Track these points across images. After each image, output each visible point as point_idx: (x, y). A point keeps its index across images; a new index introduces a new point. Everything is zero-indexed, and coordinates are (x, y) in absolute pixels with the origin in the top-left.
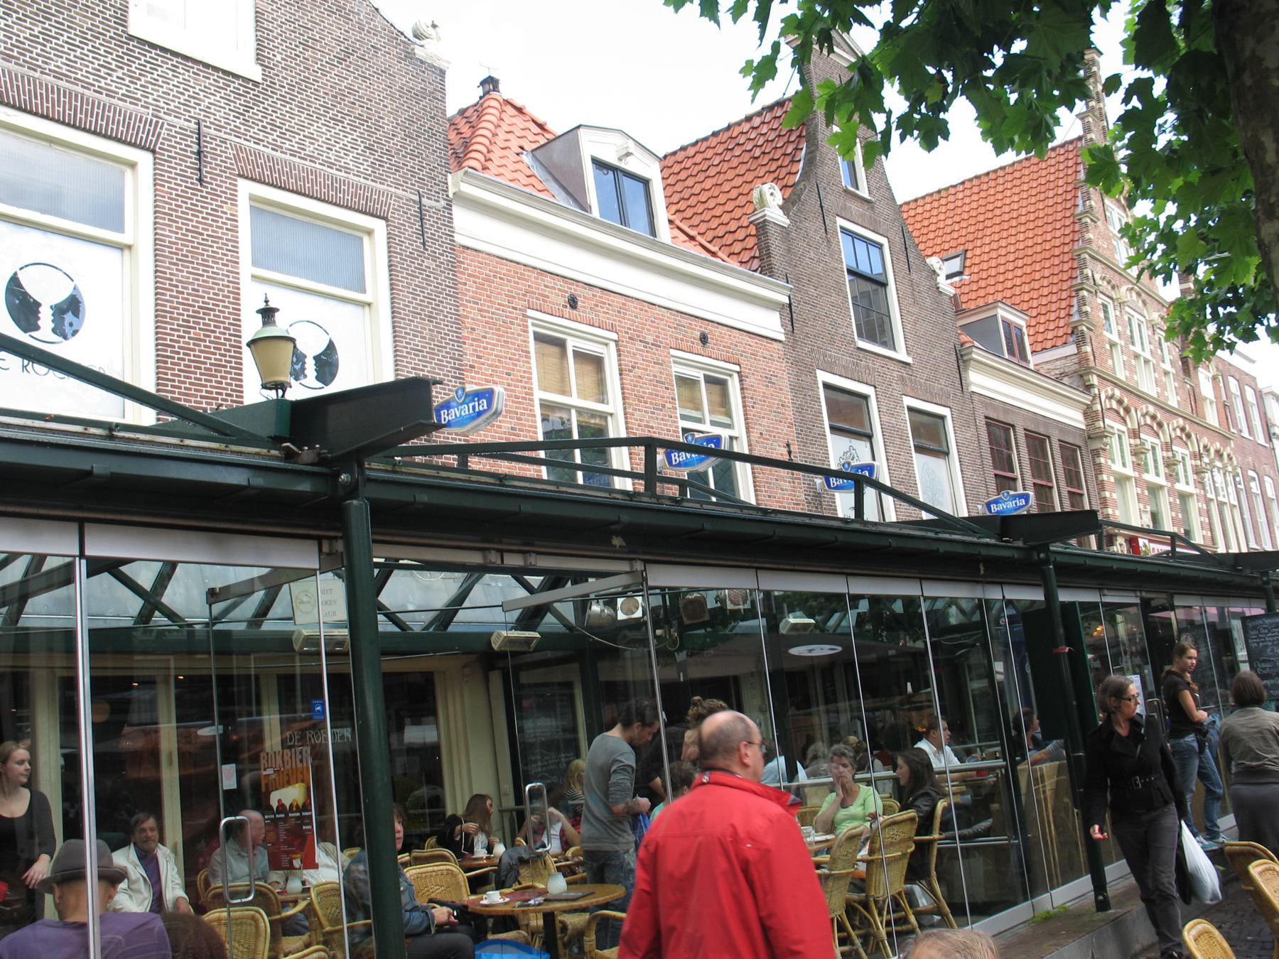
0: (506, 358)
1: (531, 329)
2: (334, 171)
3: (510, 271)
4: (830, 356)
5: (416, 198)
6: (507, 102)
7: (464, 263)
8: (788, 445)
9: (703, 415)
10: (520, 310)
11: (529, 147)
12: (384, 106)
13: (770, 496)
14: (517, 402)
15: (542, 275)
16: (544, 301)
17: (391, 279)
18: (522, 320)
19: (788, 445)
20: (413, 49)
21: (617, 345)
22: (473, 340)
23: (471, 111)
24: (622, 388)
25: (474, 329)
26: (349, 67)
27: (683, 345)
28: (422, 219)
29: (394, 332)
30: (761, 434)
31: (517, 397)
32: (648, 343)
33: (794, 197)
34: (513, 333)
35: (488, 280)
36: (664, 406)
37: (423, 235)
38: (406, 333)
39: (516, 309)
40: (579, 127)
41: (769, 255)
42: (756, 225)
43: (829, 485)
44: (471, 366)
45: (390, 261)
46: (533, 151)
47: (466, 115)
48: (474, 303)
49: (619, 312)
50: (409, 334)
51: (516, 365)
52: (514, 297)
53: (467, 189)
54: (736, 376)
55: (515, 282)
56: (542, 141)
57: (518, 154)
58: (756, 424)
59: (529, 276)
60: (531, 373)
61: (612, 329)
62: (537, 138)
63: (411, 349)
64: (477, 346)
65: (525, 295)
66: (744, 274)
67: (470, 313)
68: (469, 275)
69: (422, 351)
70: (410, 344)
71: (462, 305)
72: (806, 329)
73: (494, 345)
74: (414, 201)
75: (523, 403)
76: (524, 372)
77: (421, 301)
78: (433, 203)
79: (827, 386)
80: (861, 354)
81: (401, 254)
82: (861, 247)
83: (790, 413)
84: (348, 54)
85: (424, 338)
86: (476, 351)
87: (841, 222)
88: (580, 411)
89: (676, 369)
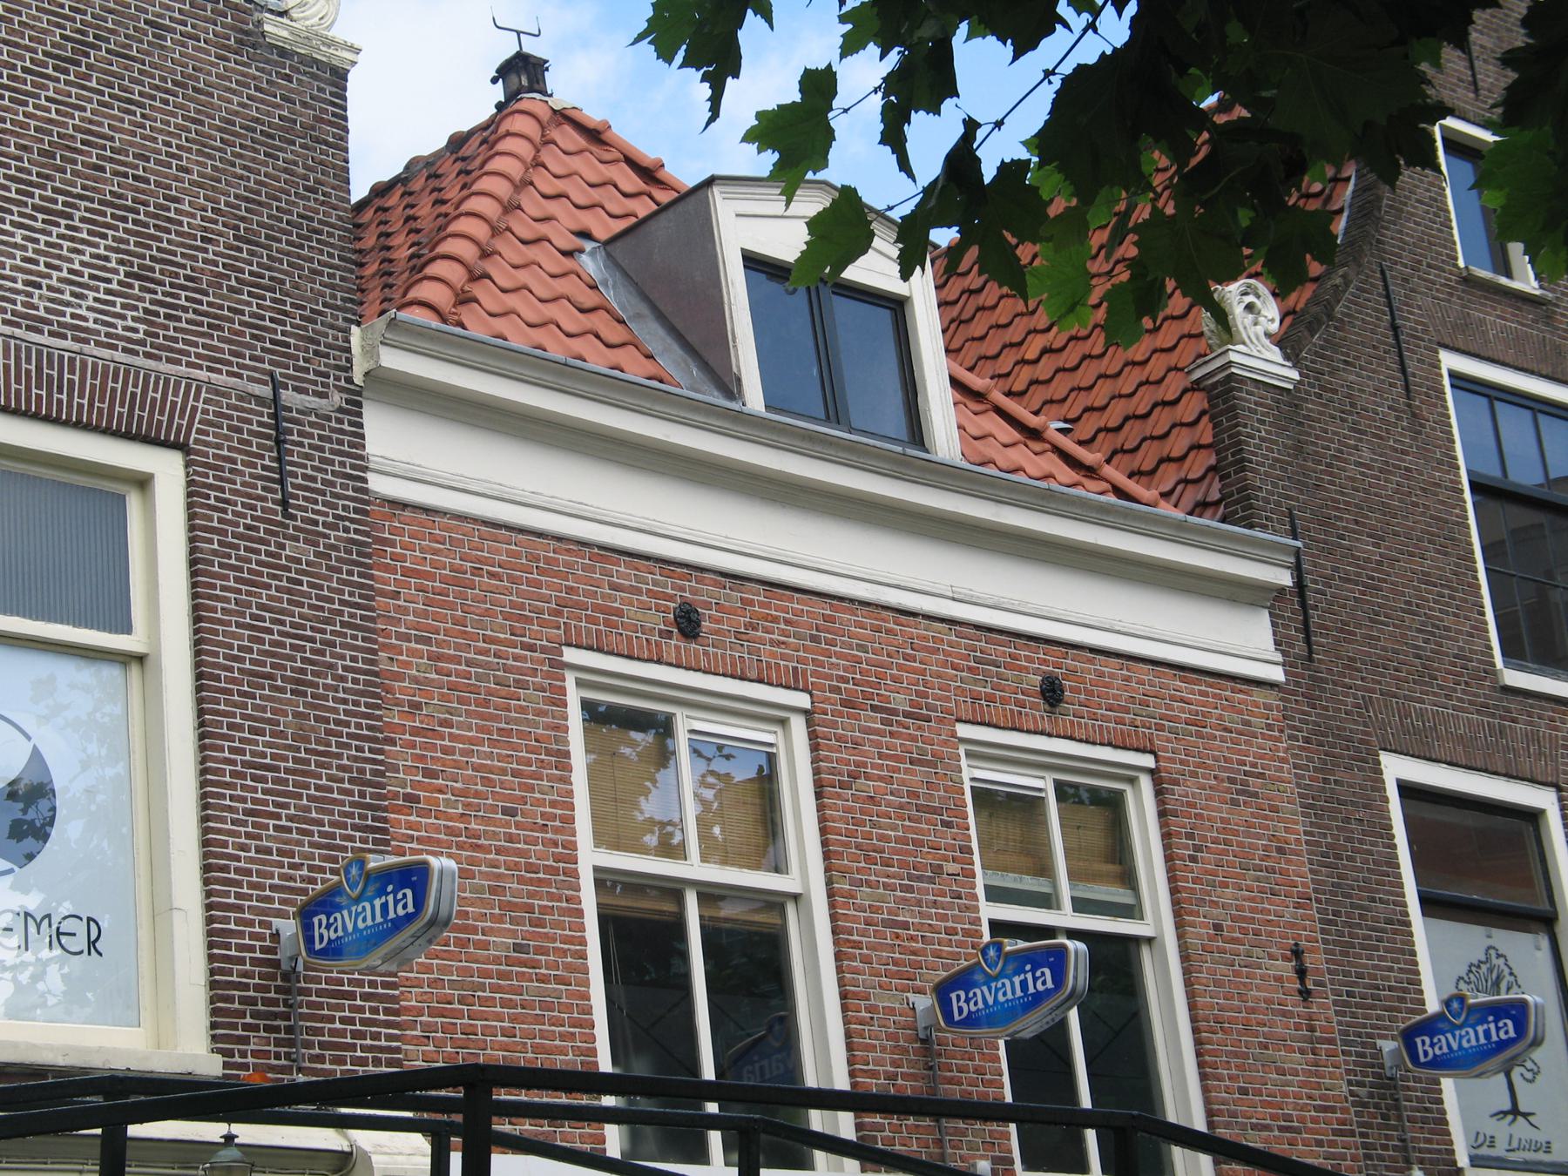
0: (503, 772)
1: (573, 697)
2: (44, 339)
3: (516, 555)
4: (1421, 714)
5: (265, 391)
6: (564, 117)
7: (392, 544)
8: (1297, 953)
9: (1055, 885)
10: (544, 650)
11: (604, 228)
12: (181, 169)
13: (1244, 1091)
14: (531, 882)
15: (603, 559)
16: (607, 623)
17: (195, 596)
18: (547, 675)
19: (1297, 953)
20: (260, 23)
21: (809, 723)
22: (416, 732)
23: (475, 142)
24: (823, 831)
25: (418, 706)
26: (88, 78)
27: (995, 711)
28: (279, 442)
29: (202, 724)
30: (1218, 927)
31: (531, 868)
32: (894, 712)
33: (1316, 309)
34: (523, 710)
35: (456, 582)
36: (938, 870)
37: (281, 482)
38: (231, 726)
39: (532, 648)
40: (710, 182)
41: (1241, 465)
42: (1208, 390)
43: (1414, 1057)
44: (408, 797)
45: (192, 551)
46: (607, 243)
47: (465, 151)
48: (419, 640)
49: (814, 639)
50: (240, 728)
51: (531, 789)
52: (528, 620)
53: (393, 360)
54: (1146, 783)
55: (530, 583)
56: (643, 208)
57: (568, 254)
58: (1201, 902)
59: (567, 564)
60: (572, 807)
61: (793, 683)
62: (632, 205)
63: (245, 764)
64: (424, 747)
65: (559, 614)
66: (1180, 526)
67: (407, 665)
68: (407, 573)
69: (276, 769)
70: (242, 752)
71: (384, 647)
72: (1350, 649)
73: (471, 741)
74: (260, 400)
75: (548, 883)
76: (553, 804)
77: (273, 643)
78: (312, 401)
79: (1409, 791)
80: (1514, 705)
81: (224, 533)
82: (1514, 423)
83: (1301, 872)
84: (83, 48)
85: (282, 735)
86: (422, 758)
87: (1450, 361)
88: (710, 895)
89: (971, 773)
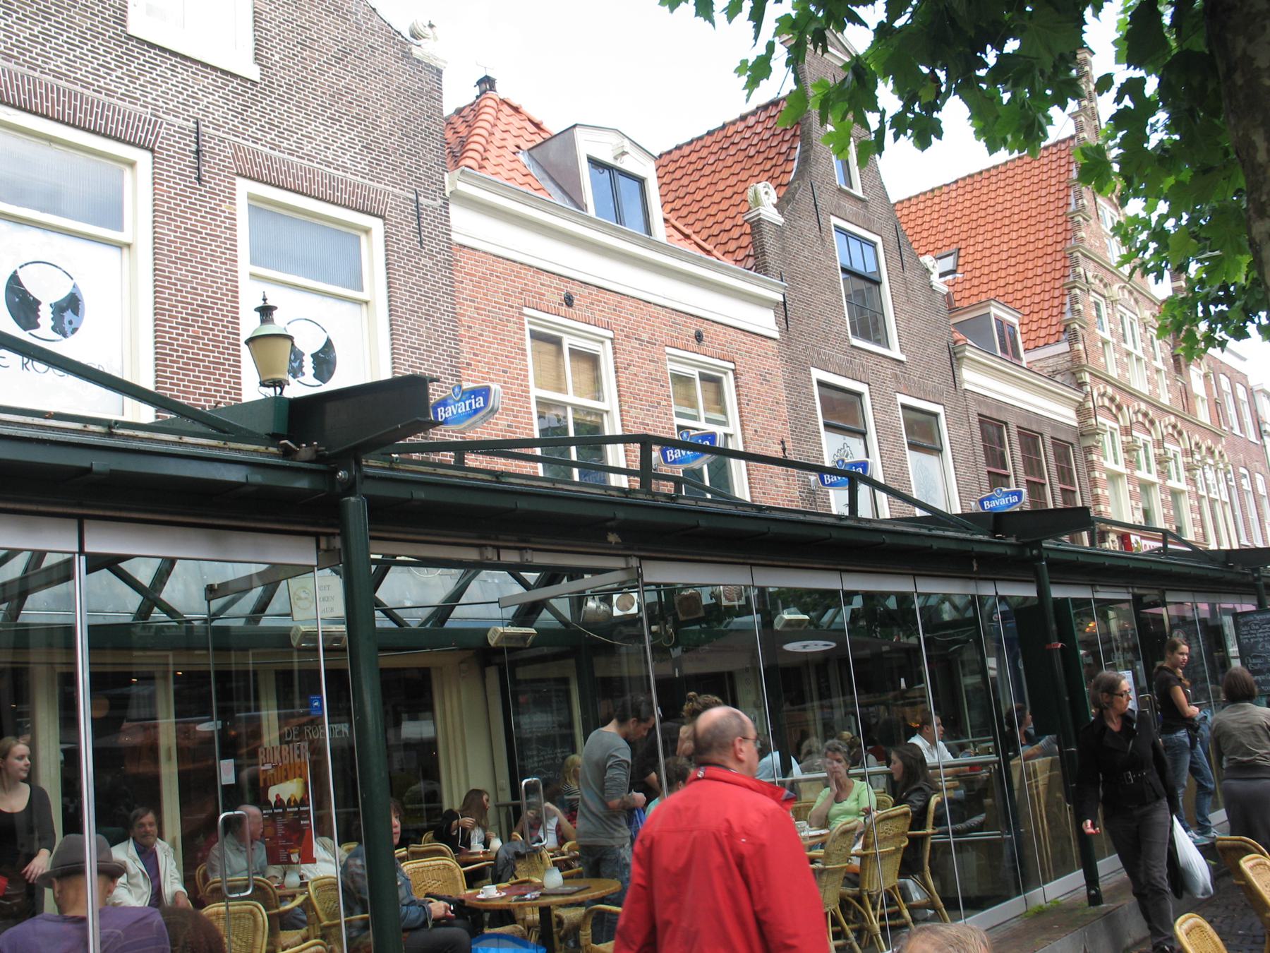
0: (502, 355)
1: (527, 327)
2: (331, 170)
3: (506, 269)
4: (824, 354)
5: (413, 197)
6: (504, 102)
7: (460, 261)
8: (783, 442)
9: (698, 412)
10: (517, 308)
11: (525, 146)
12: (382, 105)
13: (764, 493)
14: (513, 400)
15: (538, 273)
16: (540, 299)
17: (388, 278)
18: (518, 318)
19: (783, 442)
20: (410, 49)
21: (612, 343)
22: (470, 338)
23: (467, 110)
24: (618, 386)
25: (470, 327)
26: (347, 66)
27: (679, 343)
28: (419, 218)
29: (392, 330)
30: (756, 431)
31: (513, 395)
32: (643, 341)
33: (788, 196)
34: (509, 331)
35: (484, 279)
36: (659, 404)
37: (420, 234)
38: (403, 331)
39: (512, 307)
40: (574, 126)
41: (763, 253)
42: (751, 224)
43: (823, 482)
44: (468, 364)
45: (387, 260)
46: (529, 150)
47: (463, 114)
48: (471, 301)
49: (615, 310)
50: (406, 332)
51: (513, 363)
52: (510, 295)
53: (463, 187)
54: (731, 373)
55: (511, 280)
56: (539, 140)
57: (514, 153)
58: (750, 421)
59: (525, 274)
60: (527, 371)
61: (607, 327)
62: (533, 137)
63: (408, 347)
64: (473, 344)
65: (521, 293)
66: (738, 272)
67: (467, 311)
68: (466, 273)
69: (419, 349)
70: (407, 342)
71: (459, 303)
72: (801, 327)
73: (491, 343)
74: (411, 200)
75: (519, 401)
76: (521, 370)
77: (418, 299)
78: (430, 202)
79: (821, 384)
80: (855, 352)
81: (399, 253)
82: (855, 245)
83: (784, 411)
84: (346, 54)
85: (422, 336)
86: (472, 348)
87: (835, 220)
88: (576, 408)
89: (671, 367)
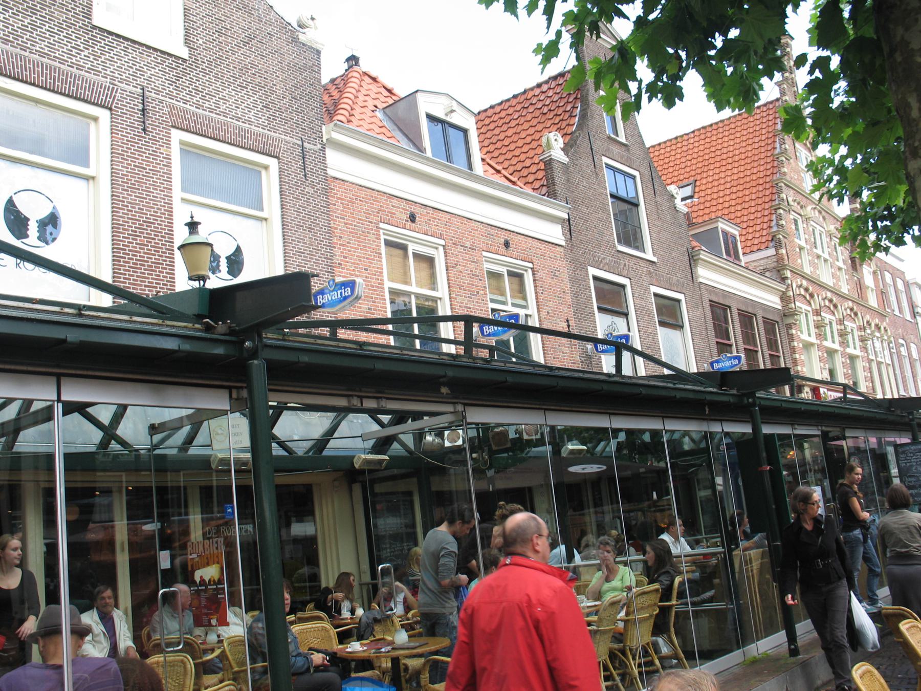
0: (364, 258)
1: (382, 237)
2: (240, 124)
3: (367, 195)
4: (598, 257)
5: (300, 143)
6: (365, 74)
7: (334, 190)
8: (568, 321)
9: (506, 299)
10: (375, 223)
11: (381, 106)
12: (277, 76)
13: (554, 358)
14: (372, 290)
15: (390, 198)
16: (391, 217)
17: (282, 201)
18: (376, 231)
19: (568, 321)
20: (297, 36)
21: (444, 249)
22: (341, 245)
23: (339, 80)
24: (448, 280)
25: (341, 237)
26: (252, 48)
27: (492, 248)
28: (304, 158)
29: (284, 239)
30: (548, 313)
31: (372, 286)
32: (466, 247)
33: (572, 142)
34: (369, 240)
35: (351, 202)
36: (478, 293)
37: (304, 170)
38: (292, 240)
39: (371, 222)
40: (417, 92)
41: (554, 184)
42: (544, 162)
43: (597, 350)
44: (339, 264)
45: (281, 188)
46: (384, 109)
47: (336, 83)
48: (341, 218)
49: (446, 225)
50: (294, 241)
51: (372, 263)
52: (370, 214)
53: (336, 136)
54: (530, 271)
55: (371, 203)
56: (391, 102)
57: (373, 111)
58: (544, 305)
59: (381, 199)
60: (382, 269)
61: (441, 237)
62: (387, 99)
63: (296, 251)
64: (343, 249)
65: (378, 213)
66: (536, 197)
67: (339, 225)
68: (338, 198)
69: (304, 253)
70: (295, 248)
71: (333, 220)
72: (581, 237)
73: (356, 248)
74: (298, 145)
75: (376, 291)
76: (378, 268)
77: (303, 217)
78: (312, 147)
79: (596, 278)
80: (620, 255)
81: (289, 183)
82: (620, 178)
83: (569, 298)
84: (251, 39)
85: (306, 243)
86: (342, 253)
87: (605, 160)
88: (418, 296)
89: (487, 266)
